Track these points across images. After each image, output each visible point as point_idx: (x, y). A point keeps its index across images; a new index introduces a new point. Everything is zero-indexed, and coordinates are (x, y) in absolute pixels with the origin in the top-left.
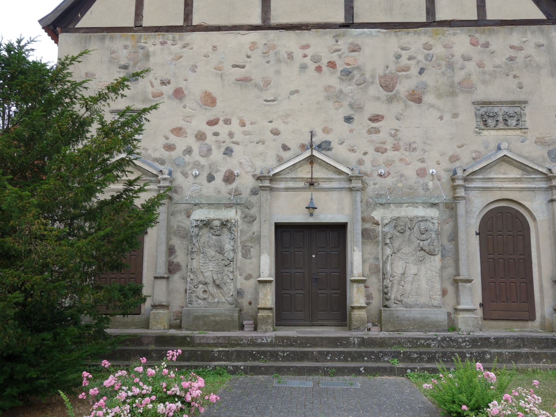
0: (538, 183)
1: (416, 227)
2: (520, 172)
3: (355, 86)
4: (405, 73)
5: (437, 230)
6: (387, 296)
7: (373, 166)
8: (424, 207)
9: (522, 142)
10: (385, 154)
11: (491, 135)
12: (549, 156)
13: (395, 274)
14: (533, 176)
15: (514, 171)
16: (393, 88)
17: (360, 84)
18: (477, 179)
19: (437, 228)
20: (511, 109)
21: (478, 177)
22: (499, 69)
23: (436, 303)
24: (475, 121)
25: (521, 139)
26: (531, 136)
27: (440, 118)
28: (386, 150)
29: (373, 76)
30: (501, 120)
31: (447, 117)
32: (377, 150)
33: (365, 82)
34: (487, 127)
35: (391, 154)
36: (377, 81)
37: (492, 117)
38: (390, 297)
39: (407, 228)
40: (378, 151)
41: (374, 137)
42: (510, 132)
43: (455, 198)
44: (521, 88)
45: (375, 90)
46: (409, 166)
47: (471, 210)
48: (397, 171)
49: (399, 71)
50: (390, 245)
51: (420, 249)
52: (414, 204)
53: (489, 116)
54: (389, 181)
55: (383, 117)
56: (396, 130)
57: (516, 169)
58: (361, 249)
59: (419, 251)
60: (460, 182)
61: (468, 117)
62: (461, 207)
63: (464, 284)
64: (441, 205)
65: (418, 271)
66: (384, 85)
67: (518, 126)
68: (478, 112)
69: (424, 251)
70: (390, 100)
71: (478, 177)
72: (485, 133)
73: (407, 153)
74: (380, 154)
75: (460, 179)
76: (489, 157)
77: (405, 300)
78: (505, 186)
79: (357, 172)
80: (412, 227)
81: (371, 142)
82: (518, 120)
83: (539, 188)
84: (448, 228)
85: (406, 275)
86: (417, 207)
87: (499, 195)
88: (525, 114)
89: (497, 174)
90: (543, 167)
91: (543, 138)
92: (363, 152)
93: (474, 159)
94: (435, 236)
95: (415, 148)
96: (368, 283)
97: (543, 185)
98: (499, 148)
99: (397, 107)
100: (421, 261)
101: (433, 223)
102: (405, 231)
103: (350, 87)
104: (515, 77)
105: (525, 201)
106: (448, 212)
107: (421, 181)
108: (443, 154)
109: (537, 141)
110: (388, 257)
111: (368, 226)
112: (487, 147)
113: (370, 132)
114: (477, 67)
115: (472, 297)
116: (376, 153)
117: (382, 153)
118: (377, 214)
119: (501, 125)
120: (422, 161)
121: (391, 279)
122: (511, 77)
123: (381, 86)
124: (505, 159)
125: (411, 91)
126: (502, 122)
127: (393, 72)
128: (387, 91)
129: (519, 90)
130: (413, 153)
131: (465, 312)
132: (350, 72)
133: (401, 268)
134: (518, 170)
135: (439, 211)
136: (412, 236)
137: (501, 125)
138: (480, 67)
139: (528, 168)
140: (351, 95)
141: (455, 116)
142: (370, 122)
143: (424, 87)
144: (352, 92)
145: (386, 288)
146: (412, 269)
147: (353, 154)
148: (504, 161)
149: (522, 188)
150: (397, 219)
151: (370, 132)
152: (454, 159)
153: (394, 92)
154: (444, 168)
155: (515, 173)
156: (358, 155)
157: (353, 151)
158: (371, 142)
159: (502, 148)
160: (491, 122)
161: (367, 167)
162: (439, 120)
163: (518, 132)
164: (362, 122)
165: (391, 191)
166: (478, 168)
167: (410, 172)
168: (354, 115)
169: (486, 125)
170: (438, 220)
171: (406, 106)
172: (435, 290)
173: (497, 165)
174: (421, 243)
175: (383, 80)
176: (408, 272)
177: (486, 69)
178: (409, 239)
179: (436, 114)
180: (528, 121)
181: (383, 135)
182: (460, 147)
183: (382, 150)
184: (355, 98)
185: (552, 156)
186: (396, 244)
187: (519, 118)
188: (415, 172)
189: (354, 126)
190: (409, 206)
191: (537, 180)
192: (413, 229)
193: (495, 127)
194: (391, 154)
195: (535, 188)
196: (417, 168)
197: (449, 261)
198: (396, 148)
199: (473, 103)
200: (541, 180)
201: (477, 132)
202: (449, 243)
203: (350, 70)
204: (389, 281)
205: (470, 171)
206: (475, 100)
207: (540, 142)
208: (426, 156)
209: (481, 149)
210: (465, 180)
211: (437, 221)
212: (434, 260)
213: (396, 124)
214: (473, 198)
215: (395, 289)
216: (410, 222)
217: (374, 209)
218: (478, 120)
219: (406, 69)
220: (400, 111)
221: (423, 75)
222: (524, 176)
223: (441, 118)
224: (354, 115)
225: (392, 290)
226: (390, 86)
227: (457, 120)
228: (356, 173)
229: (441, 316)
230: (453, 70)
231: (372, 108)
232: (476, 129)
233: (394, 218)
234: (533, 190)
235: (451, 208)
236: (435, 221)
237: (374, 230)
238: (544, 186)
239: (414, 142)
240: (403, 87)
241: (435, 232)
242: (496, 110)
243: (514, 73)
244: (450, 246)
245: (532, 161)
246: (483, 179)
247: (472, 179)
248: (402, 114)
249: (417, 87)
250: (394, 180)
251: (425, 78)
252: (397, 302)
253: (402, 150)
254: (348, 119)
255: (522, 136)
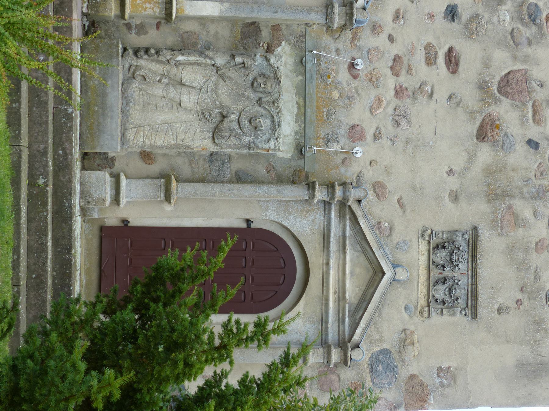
0: (336, 328)
1: (263, 112)
2: (355, 301)
3: (509, 29)
4: (530, 115)
5: (258, 147)
6: (142, 53)
7: (369, 49)
8: (296, 133)
9: (406, 308)
10: (389, 72)
11: (419, 254)
12: (381, 351)
13: (180, 68)
14: (347, 319)
15: (357, 289)
16: (506, 95)
17: (512, 37)
18: (345, 225)
19: (260, 146)
20: (463, 292)
21: (348, 228)
22: (533, 277)
23: (130, 135)
24: (444, 230)
25: (411, 306)
26: (417, 324)
27: (451, 170)
28: (397, 75)
29: (526, 59)
30: (445, 274)
31: (453, 183)
32: (397, 59)
33: (517, 44)
34: (434, 249)
35: (391, 82)
36: (518, 66)
37: (451, 259)
38: (141, 58)
39: (261, 95)
40: (394, 60)
41: (420, 56)
42: (422, 289)
43: (311, 186)
44: (499, 311)
45: (503, 62)
46: (368, 113)
47: (290, 213)
48: (360, 91)
49: (533, 106)
50: (232, 63)
51: (224, 114)
52: (302, 116)
53: (454, 257)
54: (344, 76)
55: (454, 72)
56: (431, 95)
57: (361, 293)
58: (224, 14)
59: (221, 113)
60: (339, 193)
61: (450, 218)
62: (296, 192)
63: (163, 188)
64: (301, 162)
65: (186, 109)
66: (510, 77)
67: (433, 301)
68: (459, 234)
69: (221, 122)
70: (483, 86)
71: (348, 228)
72: (423, 246)
73: (390, 110)
74: (390, 63)
75: (344, 193)
76: (381, 247)
77: (135, 85)
78: (331, 272)
79: (360, 17)
80: (263, 105)
81: (412, 50)
82: (444, 303)
83: (327, 328)
84: (261, 169)
85: (179, 87)
86: (296, 121)
87: (315, 260)
88: (453, 315)
89: (351, 260)
90: (363, 335)
91: (412, 343)
92: (394, 35)
93: (379, 224)
94: (246, 141)
95: (399, 124)
96: (164, 28)
97: (332, 336)
98: (395, 266)
99: (470, 96)
100: (203, 115)
101: (269, 140)
102: (256, 91)
103: (507, 19)
104: (519, 302)
105: (306, 306)
106: (288, 173)
107: (342, 132)
108: (388, 171)
109: (408, 332)
110: (211, 58)
111: (265, 34)
112: (398, 245)
113: (428, 47)
114: (537, 240)
115: (142, 208)
116: (392, 57)
117: (392, 68)
118: (284, 57)
119: (436, 273)
120: (377, 136)
121: (172, 62)
122: (520, 296)
123: (509, 73)
124: (378, 273)
125: (498, 123)
126: (440, 276)
127: (533, 95)
128: (499, 84)
129: (496, 307)
130: (390, 120)
131: (114, 186)
132: (534, 20)
133: (192, 79)
134: (358, 298)
135: (290, 160)
136: (247, 103)
137: (436, 273)
138: (537, 244)
139: (361, 313)
140: (495, 19)
141: (455, 198)
142: (446, 48)
143: (504, 146)
144: (499, 22)
145: (157, 53)
146: (189, 100)
147: (389, 17)
148: (375, 273)
149: (327, 300)
150: (277, 79)
151: (428, 47)
152: (379, 189)
153: (498, 95)
154: (364, 171)
155: (352, 291)
156: (389, 27)
157: (397, 17)
158: (412, 50)
159: (396, 270)
160: (441, 256)
161: (367, 40)
162: (446, 169)
163: (423, 302)
164: (446, 36)
165: (324, 76)
166: (363, 227)
167: (358, 114)
168: (460, 22)
169: (437, 247)
170: (275, 150)
171: (472, 114)
172: (153, 136)
173: (366, 262)
174: (234, 117)
175: (518, 76)
176: (185, 90)
177: (534, 255)
178: (242, 95)
179: (458, 164)
180: (441, 320)
181: (422, 70)
182: (399, 201)
183: (398, 68)
184: (490, 26)
185: (380, 357)
186: (232, 74)
187: (447, 304)
188: (357, 122)
189: (440, 22)
190: (299, 107)
191: (341, 327)
192: (259, 105)
193: (433, 262)
194: (391, 82)
195: (327, 322)
196: (364, 125)
197: (202, 167)
198: (399, 92)
199: (475, 229)
200: (340, 333)
201: (424, 231)
202: (234, 173)
203: (538, 21)
204: (168, 57)
205: (359, 213)
206: (480, 232)
207: (405, 340)
208: (385, 142)
209: (396, 238)
210: (343, 204)
211: (273, 147)
212: (204, 138)
213: (441, 95)
214: (311, 218)
215: (154, 66)
216: (271, 100)
217: (295, 46)
218: (446, 236)
219: (537, 118)
220: (464, 102)
221: (526, 147)
222: (347, 306)
223: (450, 172)
224: (460, 22)
225: (153, 61)
226: (508, 89)
227: (447, 199)
228: (358, 16)
229: (110, 145)
230: (533, 198)
231: (470, 53)
232: (430, 231)
233: (279, 74)
234: (324, 319)
235: (299, 176)
236: (272, 143)
237: (257, 45)
238: (330, 336)
239: (409, 123)
240: (505, 111)
241: (253, 143)
242: (463, 266)
243: (526, 302)
244: (229, 171)
245: (378, 309)
246: (344, 236)
247: (344, 217)
248: (458, 104)
249: (506, 134)
250: (345, 85)
251: (521, 148)
252: (131, 70)
253: (396, 102)
254: (452, 13)
255: (416, 307)
